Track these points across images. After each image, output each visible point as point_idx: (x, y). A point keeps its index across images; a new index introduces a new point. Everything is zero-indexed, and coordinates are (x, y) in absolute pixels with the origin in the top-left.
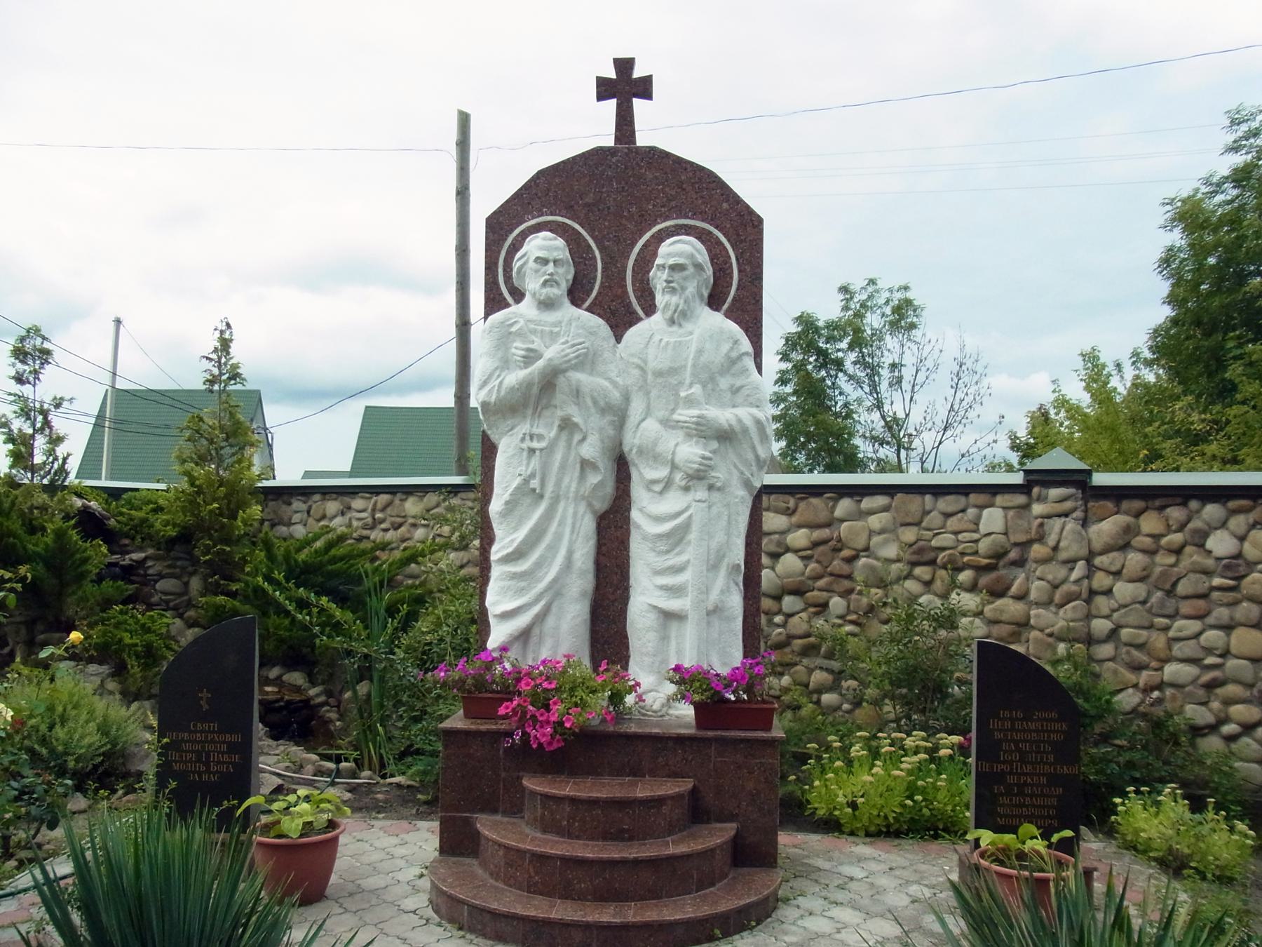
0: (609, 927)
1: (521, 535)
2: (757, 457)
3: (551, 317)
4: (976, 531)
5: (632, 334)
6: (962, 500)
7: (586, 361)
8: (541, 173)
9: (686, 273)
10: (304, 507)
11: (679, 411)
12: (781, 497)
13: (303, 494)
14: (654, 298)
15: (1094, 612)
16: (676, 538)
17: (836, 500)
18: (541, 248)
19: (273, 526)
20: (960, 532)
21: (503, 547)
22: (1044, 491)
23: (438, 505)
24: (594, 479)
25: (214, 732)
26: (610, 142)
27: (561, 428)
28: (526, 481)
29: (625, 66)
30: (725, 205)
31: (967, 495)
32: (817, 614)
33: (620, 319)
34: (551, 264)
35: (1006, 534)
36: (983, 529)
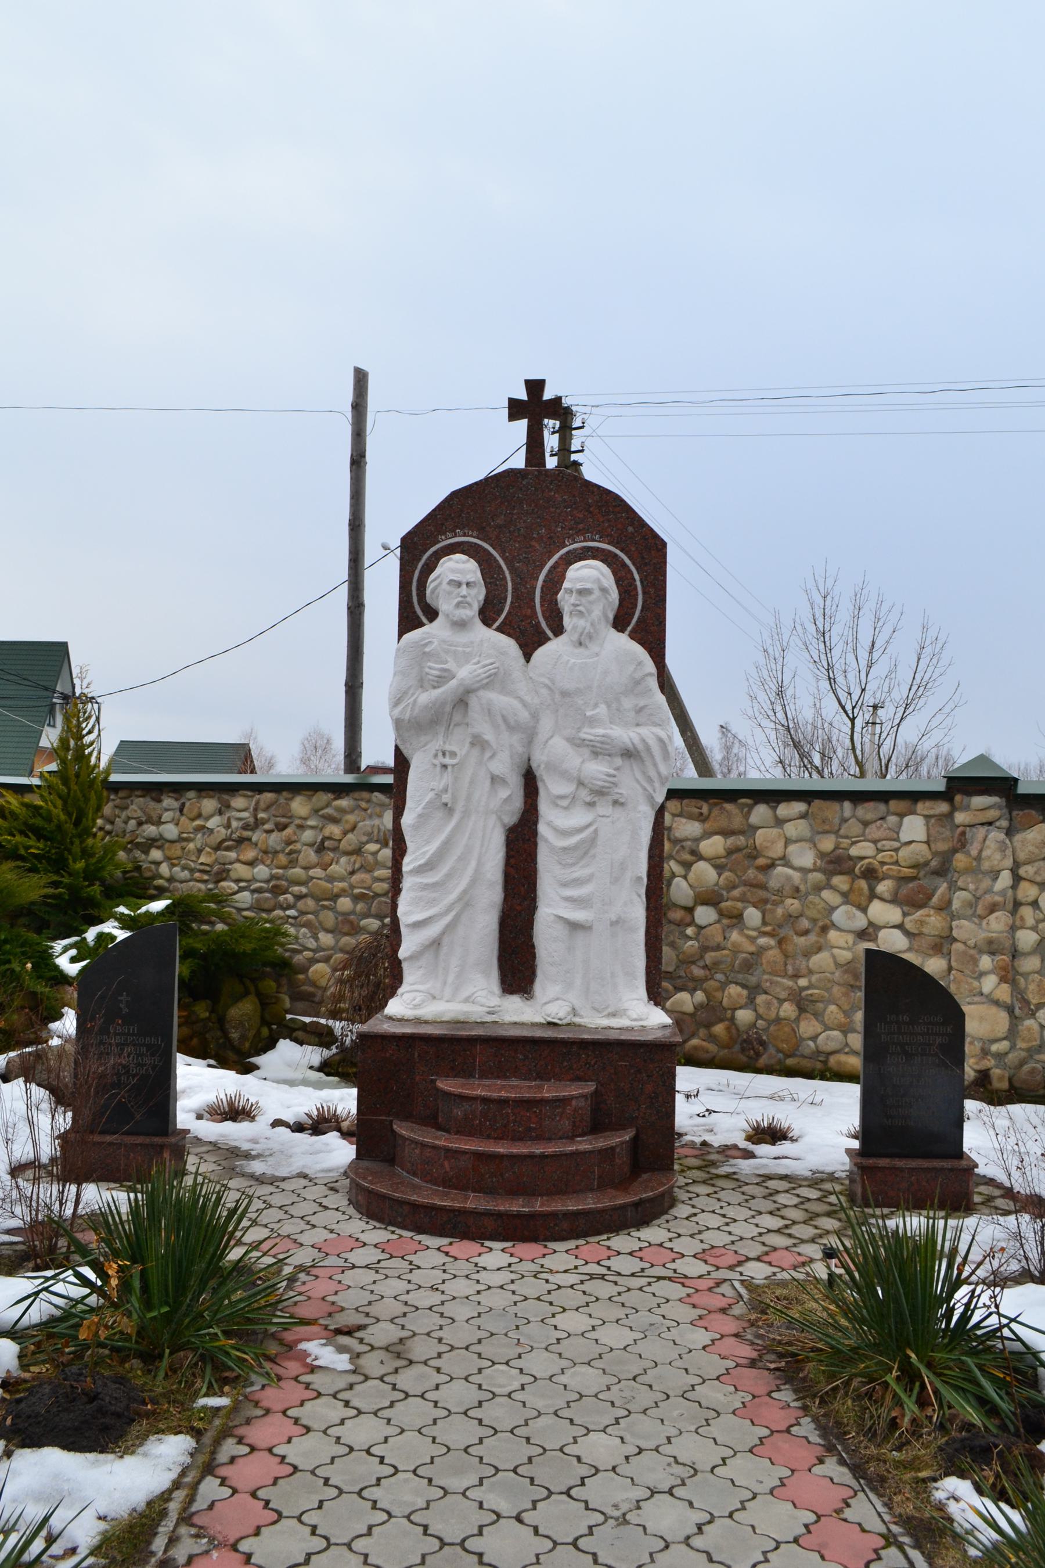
0: (519, 1216)
1: (432, 848)
2: (659, 773)
3: (463, 638)
4: (897, 840)
5: (541, 654)
6: (882, 807)
7: (494, 680)
8: (454, 494)
9: (592, 597)
10: (176, 805)
11: (585, 730)
12: (694, 802)
13: (174, 791)
14: (561, 618)
15: (1018, 923)
16: (585, 850)
17: (751, 808)
18: (457, 574)
19: (140, 824)
20: (879, 841)
21: (415, 859)
22: (966, 799)
23: (327, 806)
24: (504, 793)
25: (133, 1035)
26: (519, 462)
27: (472, 744)
28: (438, 795)
29: (535, 387)
30: (630, 529)
31: (886, 802)
32: (731, 927)
33: (530, 642)
34: (464, 586)
35: (928, 843)
36: (904, 837)
